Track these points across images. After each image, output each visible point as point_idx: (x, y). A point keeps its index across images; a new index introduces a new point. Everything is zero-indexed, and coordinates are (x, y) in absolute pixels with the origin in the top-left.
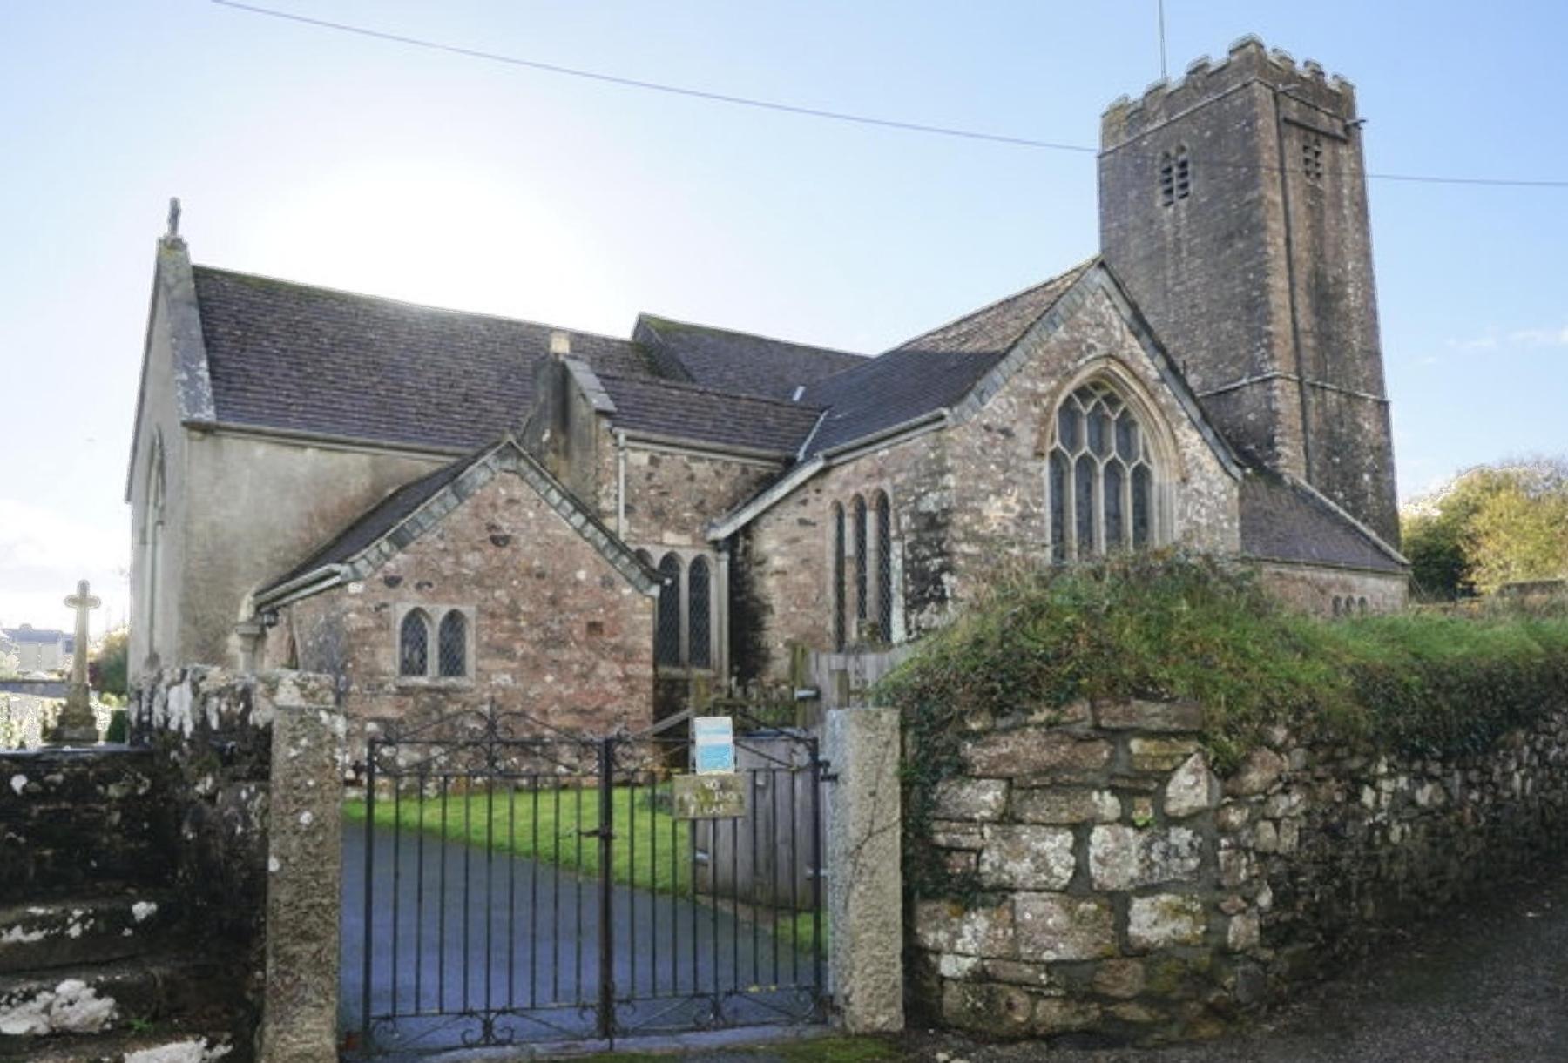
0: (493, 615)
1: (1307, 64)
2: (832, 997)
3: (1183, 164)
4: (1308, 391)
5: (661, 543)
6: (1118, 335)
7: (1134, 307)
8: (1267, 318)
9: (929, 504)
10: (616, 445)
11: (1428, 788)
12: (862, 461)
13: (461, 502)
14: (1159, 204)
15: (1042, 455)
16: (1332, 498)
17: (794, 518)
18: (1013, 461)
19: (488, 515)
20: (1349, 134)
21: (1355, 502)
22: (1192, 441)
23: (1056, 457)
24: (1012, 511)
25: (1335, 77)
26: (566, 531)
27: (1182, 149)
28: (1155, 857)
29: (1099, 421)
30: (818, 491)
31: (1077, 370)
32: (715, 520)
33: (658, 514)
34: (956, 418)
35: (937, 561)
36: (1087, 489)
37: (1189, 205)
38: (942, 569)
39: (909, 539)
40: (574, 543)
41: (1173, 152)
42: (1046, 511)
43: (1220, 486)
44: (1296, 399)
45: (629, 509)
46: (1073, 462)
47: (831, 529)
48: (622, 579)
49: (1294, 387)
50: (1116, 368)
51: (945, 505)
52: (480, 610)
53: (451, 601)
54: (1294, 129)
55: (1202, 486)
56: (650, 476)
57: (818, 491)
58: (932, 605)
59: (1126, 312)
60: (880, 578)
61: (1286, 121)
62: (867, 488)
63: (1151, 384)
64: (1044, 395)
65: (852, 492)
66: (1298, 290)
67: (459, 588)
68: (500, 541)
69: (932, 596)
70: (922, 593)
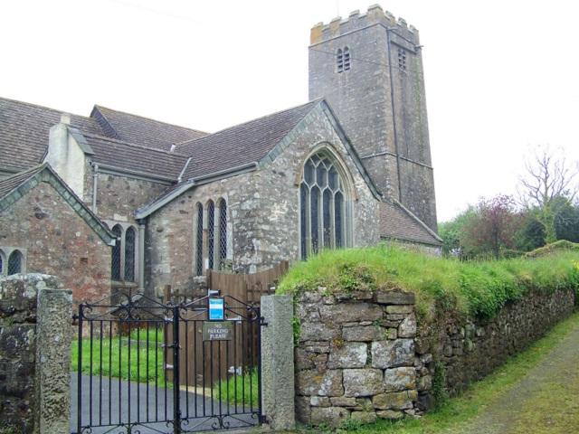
0: (35, 253)
1: (400, 19)
2: (265, 417)
3: (348, 55)
4: (400, 161)
5: (113, 220)
6: (330, 133)
7: (336, 120)
8: (383, 127)
9: (247, 205)
10: (93, 171)
11: (480, 330)
12: (213, 184)
13: (22, 196)
14: (336, 72)
15: (297, 185)
16: (410, 210)
17: (177, 209)
18: (285, 188)
19: (35, 203)
20: (416, 51)
21: (420, 212)
22: (360, 183)
23: (303, 187)
24: (284, 210)
25: (411, 26)
26: (71, 212)
27: (346, 49)
28: (398, 353)
29: (321, 171)
30: (190, 197)
31: (313, 148)
32: (139, 209)
33: (112, 205)
34: (260, 167)
35: (250, 233)
36: (315, 203)
37: (349, 74)
38: (252, 237)
39: (237, 222)
40: (74, 218)
41: (343, 49)
42: (299, 211)
43: (372, 203)
44: (395, 165)
45: (98, 202)
46: (310, 189)
47: (196, 216)
48: (97, 236)
49: (395, 159)
50: (330, 148)
51: (255, 207)
52: (29, 251)
53: (15, 246)
54: (395, 47)
55: (365, 203)
56: (109, 186)
57: (190, 197)
58: (248, 254)
59: (333, 123)
60: (198, 237)
61: (392, 43)
62: (215, 198)
63: (344, 156)
64: (298, 158)
65: (207, 198)
66: (396, 116)
67: (19, 240)
68: (39, 216)
69: (247, 249)
70: (242, 247)
